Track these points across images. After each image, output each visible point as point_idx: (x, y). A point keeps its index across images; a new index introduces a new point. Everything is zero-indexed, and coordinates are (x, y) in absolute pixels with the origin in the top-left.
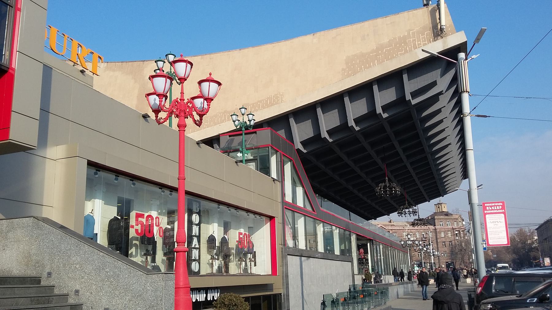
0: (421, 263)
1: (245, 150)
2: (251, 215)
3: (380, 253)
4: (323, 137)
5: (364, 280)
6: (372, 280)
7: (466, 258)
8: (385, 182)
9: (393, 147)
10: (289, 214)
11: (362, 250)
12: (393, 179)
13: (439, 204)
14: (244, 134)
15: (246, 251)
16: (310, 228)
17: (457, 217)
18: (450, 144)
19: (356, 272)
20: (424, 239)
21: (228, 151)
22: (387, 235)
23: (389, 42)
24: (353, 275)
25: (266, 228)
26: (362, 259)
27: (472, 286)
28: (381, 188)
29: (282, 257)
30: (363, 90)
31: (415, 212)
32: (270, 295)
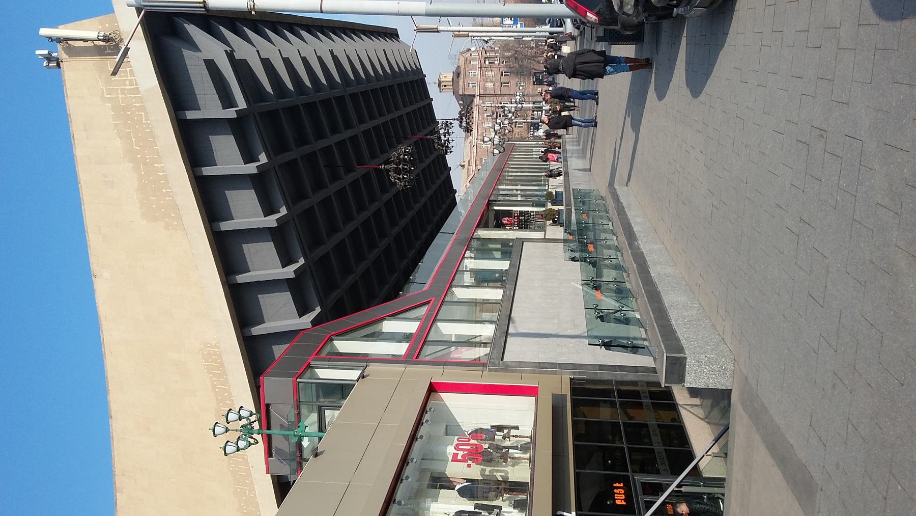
0: (532, 124)
1: (298, 432)
2: (423, 430)
3: (512, 190)
4: (292, 276)
5: (554, 222)
6: (556, 208)
7: (529, 52)
8: (388, 171)
9: (327, 150)
10: (429, 350)
11: (505, 220)
12: (385, 156)
13: (439, 85)
14: (269, 432)
15: (488, 446)
16: (459, 312)
17: (462, 59)
18: (332, 52)
19: (539, 235)
20: (495, 115)
21: (298, 459)
22: (485, 174)
23: (121, 138)
24: (545, 240)
25: (450, 400)
26: (520, 221)
27: (576, 43)
28: (399, 179)
29: (506, 371)
30: (210, 196)
31: (447, 125)
32: (573, 401)
